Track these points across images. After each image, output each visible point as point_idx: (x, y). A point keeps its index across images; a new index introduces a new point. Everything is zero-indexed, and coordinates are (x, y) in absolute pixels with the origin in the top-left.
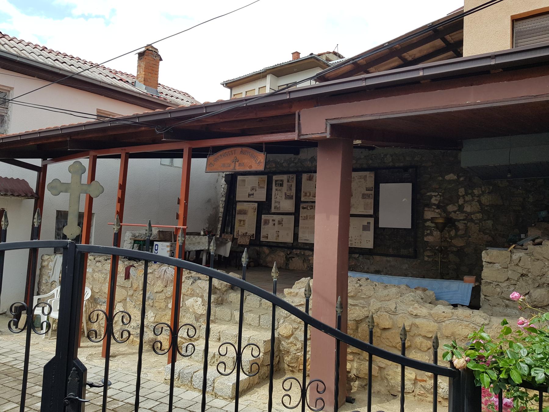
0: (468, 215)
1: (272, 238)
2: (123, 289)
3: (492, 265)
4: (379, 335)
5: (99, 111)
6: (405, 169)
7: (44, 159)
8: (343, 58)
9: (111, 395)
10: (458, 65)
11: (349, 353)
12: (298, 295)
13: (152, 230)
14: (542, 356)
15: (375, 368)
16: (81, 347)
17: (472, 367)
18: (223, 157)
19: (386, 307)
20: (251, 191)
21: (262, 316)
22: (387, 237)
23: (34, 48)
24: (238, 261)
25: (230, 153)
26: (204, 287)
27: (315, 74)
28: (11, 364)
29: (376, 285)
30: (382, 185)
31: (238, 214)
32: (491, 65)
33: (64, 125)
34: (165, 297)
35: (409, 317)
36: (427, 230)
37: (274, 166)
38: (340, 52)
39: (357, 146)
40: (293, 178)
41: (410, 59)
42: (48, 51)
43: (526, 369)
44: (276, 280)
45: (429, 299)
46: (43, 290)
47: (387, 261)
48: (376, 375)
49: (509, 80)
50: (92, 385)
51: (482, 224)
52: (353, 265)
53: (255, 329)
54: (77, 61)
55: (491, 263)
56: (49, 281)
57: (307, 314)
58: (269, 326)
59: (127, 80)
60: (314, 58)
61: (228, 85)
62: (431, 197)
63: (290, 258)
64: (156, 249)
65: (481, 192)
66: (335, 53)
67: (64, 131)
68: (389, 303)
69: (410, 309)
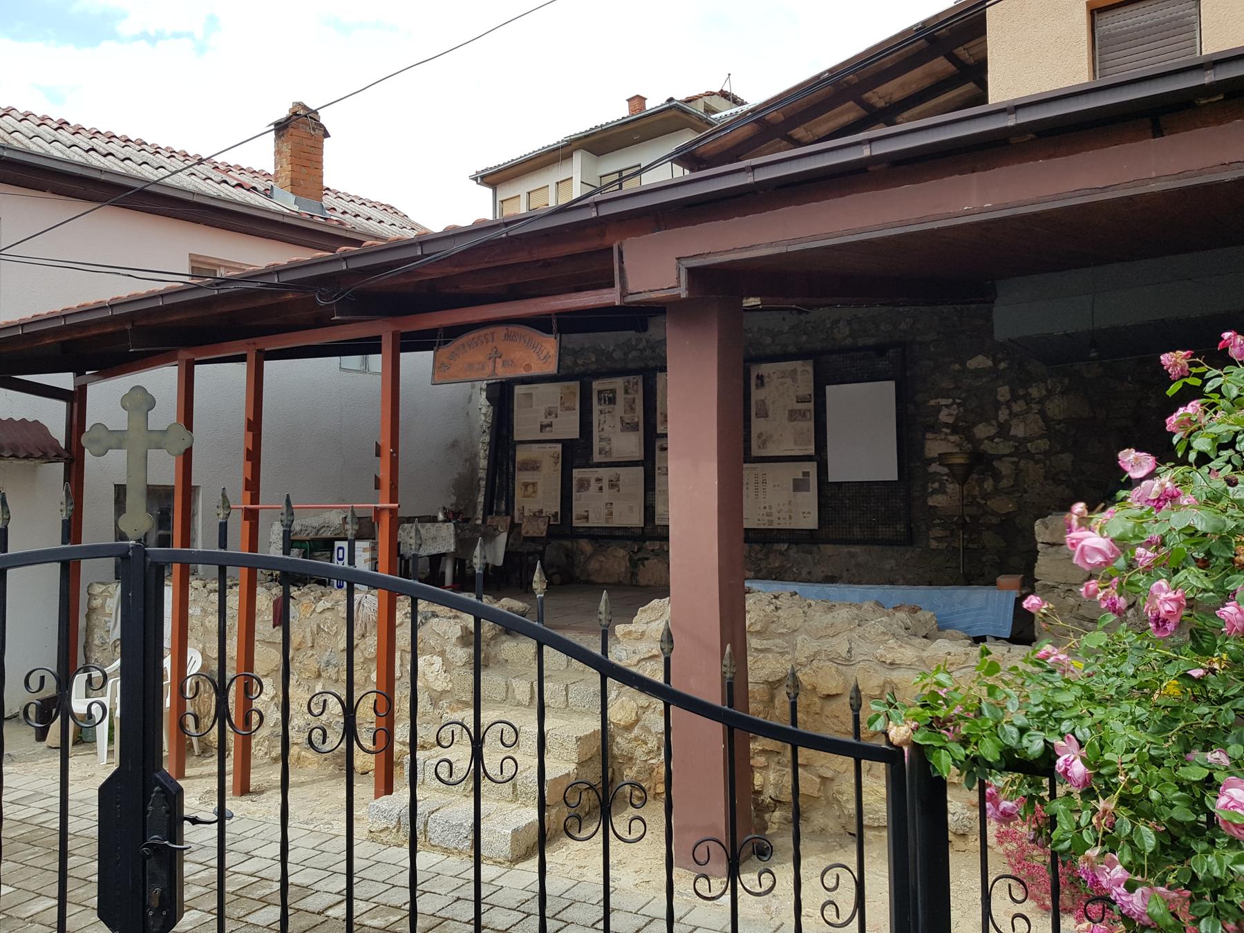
0: (1020, 444)
1: (597, 520)
2: (271, 647)
3: (1055, 548)
4: (818, 711)
5: (195, 258)
6: (880, 350)
7: (79, 372)
8: (743, 103)
9: (255, 871)
10: (920, 134)
11: (757, 753)
12: (646, 637)
13: (293, 514)
14: (1041, 708)
15: (813, 780)
16: (188, 778)
17: (921, 740)
18: (467, 347)
19: (829, 649)
20: (546, 417)
21: (571, 687)
22: (847, 501)
23: (39, 126)
24: (523, 573)
25: (482, 338)
26: (445, 633)
27: (673, 149)
28: (36, 821)
29: (810, 606)
30: (830, 389)
31: (520, 470)
32: (1007, 127)
33: (116, 297)
34: (362, 660)
35: (878, 668)
36: (933, 483)
37: (593, 359)
38: (737, 92)
39: (753, 309)
40: (637, 384)
41: (881, 104)
42: (71, 130)
43: (1015, 736)
44: (542, 595)
45: (924, 629)
46: (96, 660)
47: (849, 553)
48: (816, 796)
49: (1049, 157)
50: (195, 821)
51: (1051, 461)
52: (777, 568)
53: (558, 714)
54: (139, 148)
55: (1053, 545)
56: (108, 641)
57: (604, 657)
58: (587, 707)
59: (254, 185)
60: (676, 107)
61: (487, 180)
62: (938, 409)
63: (639, 560)
64: (341, 556)
65: (1044, 392)
66: (724, 95)
67: (117, 311)
68: (835, 641)
69: (880, 651)
